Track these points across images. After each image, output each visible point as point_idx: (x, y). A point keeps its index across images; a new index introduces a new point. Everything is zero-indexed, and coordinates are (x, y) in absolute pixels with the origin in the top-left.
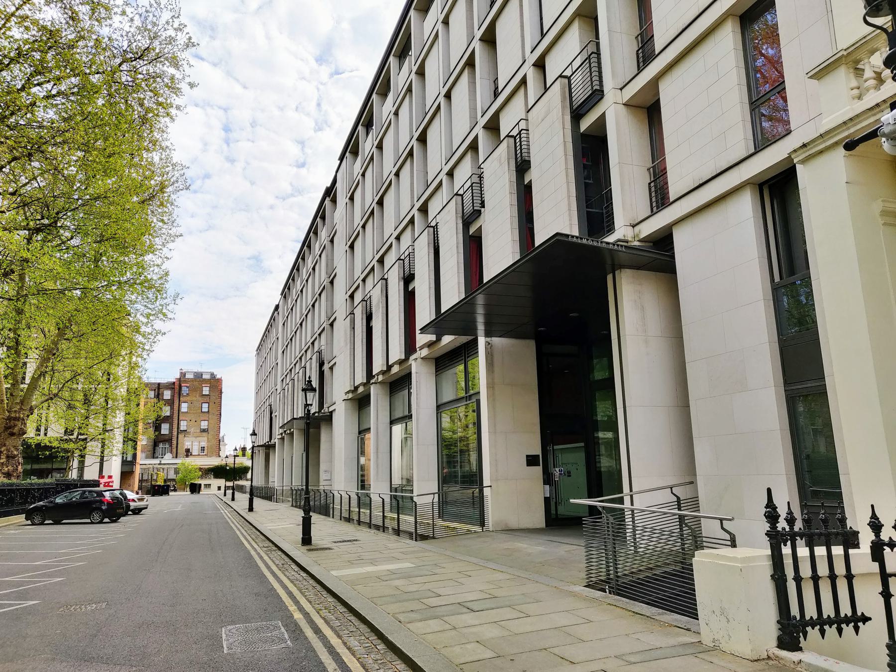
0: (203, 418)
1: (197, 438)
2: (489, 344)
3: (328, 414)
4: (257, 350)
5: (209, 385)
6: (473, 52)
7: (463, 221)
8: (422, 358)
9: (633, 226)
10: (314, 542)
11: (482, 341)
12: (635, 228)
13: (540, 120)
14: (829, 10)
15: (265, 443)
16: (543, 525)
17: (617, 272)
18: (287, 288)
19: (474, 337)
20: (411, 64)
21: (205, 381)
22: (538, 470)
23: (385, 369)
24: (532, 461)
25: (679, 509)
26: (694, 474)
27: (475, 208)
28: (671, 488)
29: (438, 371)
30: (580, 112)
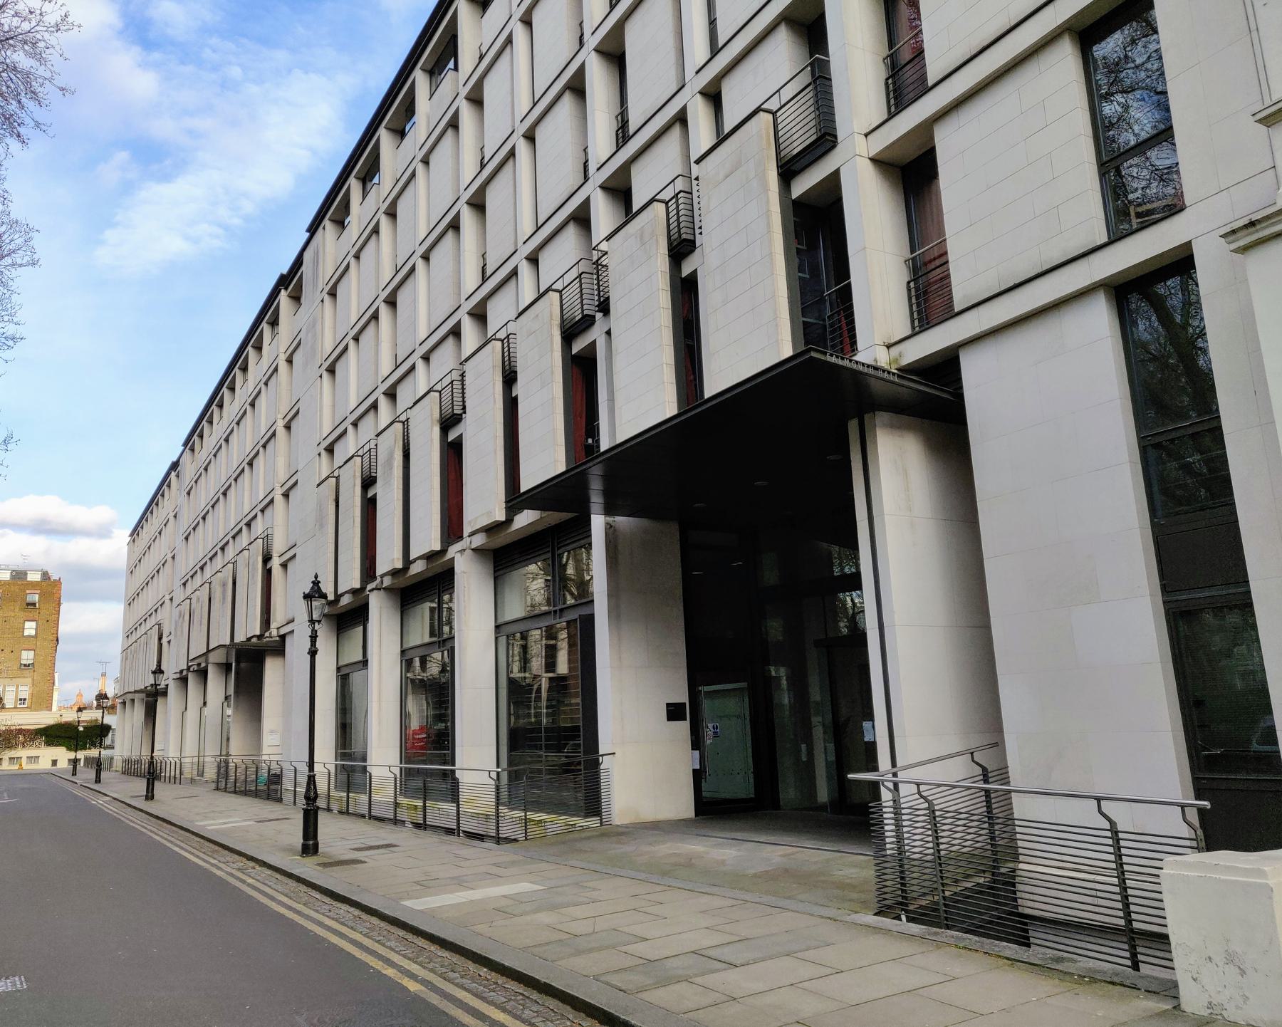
0: (27, 647)
1: (14, 679)
2: (611, 526)
3: (278, 639)
4: (132, 535)
5: (38, 592)
6: (457, 112)
7: (563, 333)
8: (472, 549)
9: (889, 347)
10: (328, 850)
11: (598, 522)
12: (892, 349)
13: (721, 176)
14: (1253, 27)
15: (146, 688)
16: (691, 813)
17: (867, 417)
18: (196, 432)
19: (565, 516)
20: (454, 83)
21: (34, 585)
22: (683, 727)
23: (399, 565)
24: (674, 712)
25: (986, 781)
26: (1000, 730)
27: (585, 312)
28: (972, 754)
29: (499, 570)
30: (793, 168)
